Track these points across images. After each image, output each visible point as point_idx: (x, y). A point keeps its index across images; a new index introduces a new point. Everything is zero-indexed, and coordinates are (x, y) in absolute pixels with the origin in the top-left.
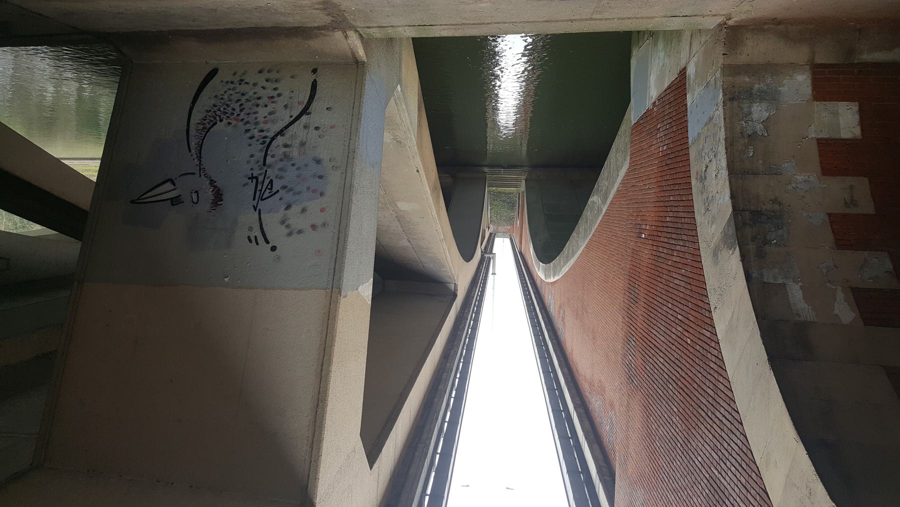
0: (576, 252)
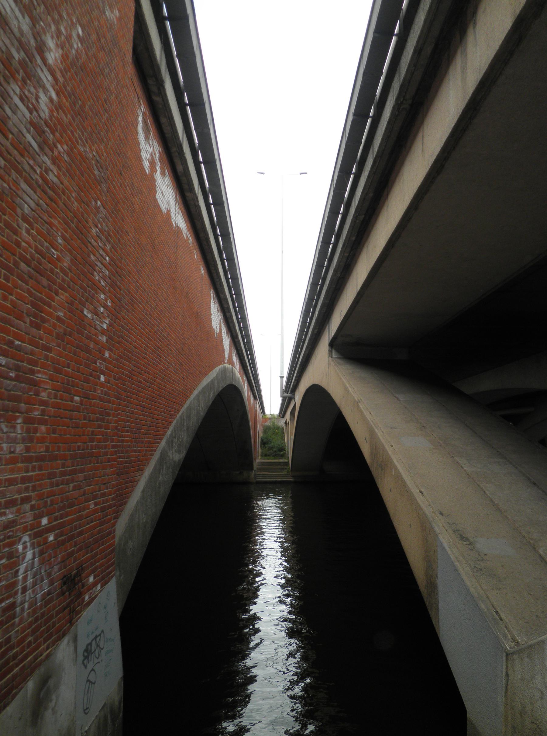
0: (200, 393)
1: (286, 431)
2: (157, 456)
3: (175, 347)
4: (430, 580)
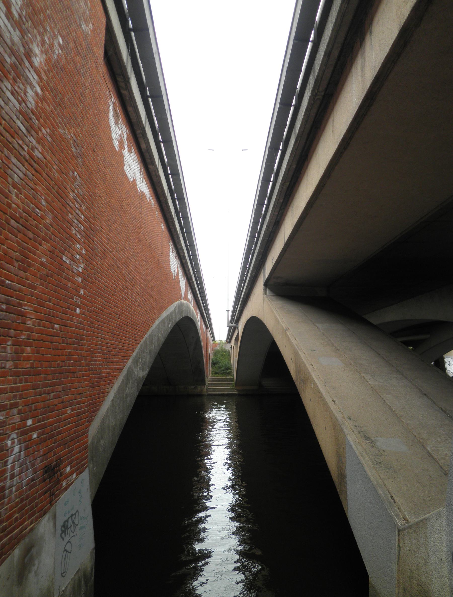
0: (160, 323)
1: (232, 355)
2: (124, 372)
3: (139, 286)
4: (341, 471)
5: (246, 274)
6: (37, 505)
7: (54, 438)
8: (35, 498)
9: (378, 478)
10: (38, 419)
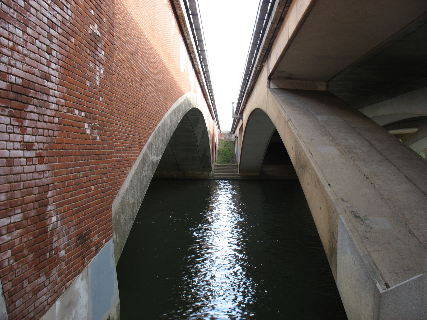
0: (172, 113)
1: (236, 144)
2: (141, 156)
3: (153, 78)
4: (332, 245)
5: (251, 68)
6: (72, 266)
7: (84, 211)
8: (70, 260)
9: (365, 250)
10: (71, 194)
